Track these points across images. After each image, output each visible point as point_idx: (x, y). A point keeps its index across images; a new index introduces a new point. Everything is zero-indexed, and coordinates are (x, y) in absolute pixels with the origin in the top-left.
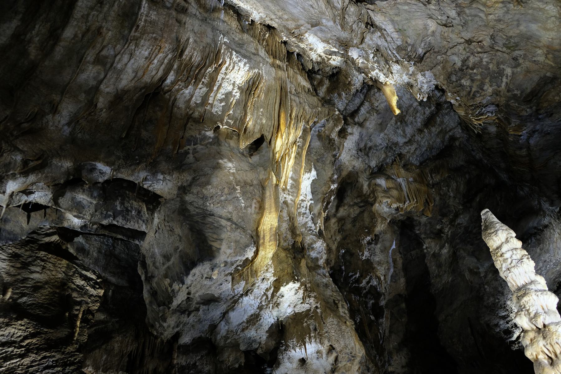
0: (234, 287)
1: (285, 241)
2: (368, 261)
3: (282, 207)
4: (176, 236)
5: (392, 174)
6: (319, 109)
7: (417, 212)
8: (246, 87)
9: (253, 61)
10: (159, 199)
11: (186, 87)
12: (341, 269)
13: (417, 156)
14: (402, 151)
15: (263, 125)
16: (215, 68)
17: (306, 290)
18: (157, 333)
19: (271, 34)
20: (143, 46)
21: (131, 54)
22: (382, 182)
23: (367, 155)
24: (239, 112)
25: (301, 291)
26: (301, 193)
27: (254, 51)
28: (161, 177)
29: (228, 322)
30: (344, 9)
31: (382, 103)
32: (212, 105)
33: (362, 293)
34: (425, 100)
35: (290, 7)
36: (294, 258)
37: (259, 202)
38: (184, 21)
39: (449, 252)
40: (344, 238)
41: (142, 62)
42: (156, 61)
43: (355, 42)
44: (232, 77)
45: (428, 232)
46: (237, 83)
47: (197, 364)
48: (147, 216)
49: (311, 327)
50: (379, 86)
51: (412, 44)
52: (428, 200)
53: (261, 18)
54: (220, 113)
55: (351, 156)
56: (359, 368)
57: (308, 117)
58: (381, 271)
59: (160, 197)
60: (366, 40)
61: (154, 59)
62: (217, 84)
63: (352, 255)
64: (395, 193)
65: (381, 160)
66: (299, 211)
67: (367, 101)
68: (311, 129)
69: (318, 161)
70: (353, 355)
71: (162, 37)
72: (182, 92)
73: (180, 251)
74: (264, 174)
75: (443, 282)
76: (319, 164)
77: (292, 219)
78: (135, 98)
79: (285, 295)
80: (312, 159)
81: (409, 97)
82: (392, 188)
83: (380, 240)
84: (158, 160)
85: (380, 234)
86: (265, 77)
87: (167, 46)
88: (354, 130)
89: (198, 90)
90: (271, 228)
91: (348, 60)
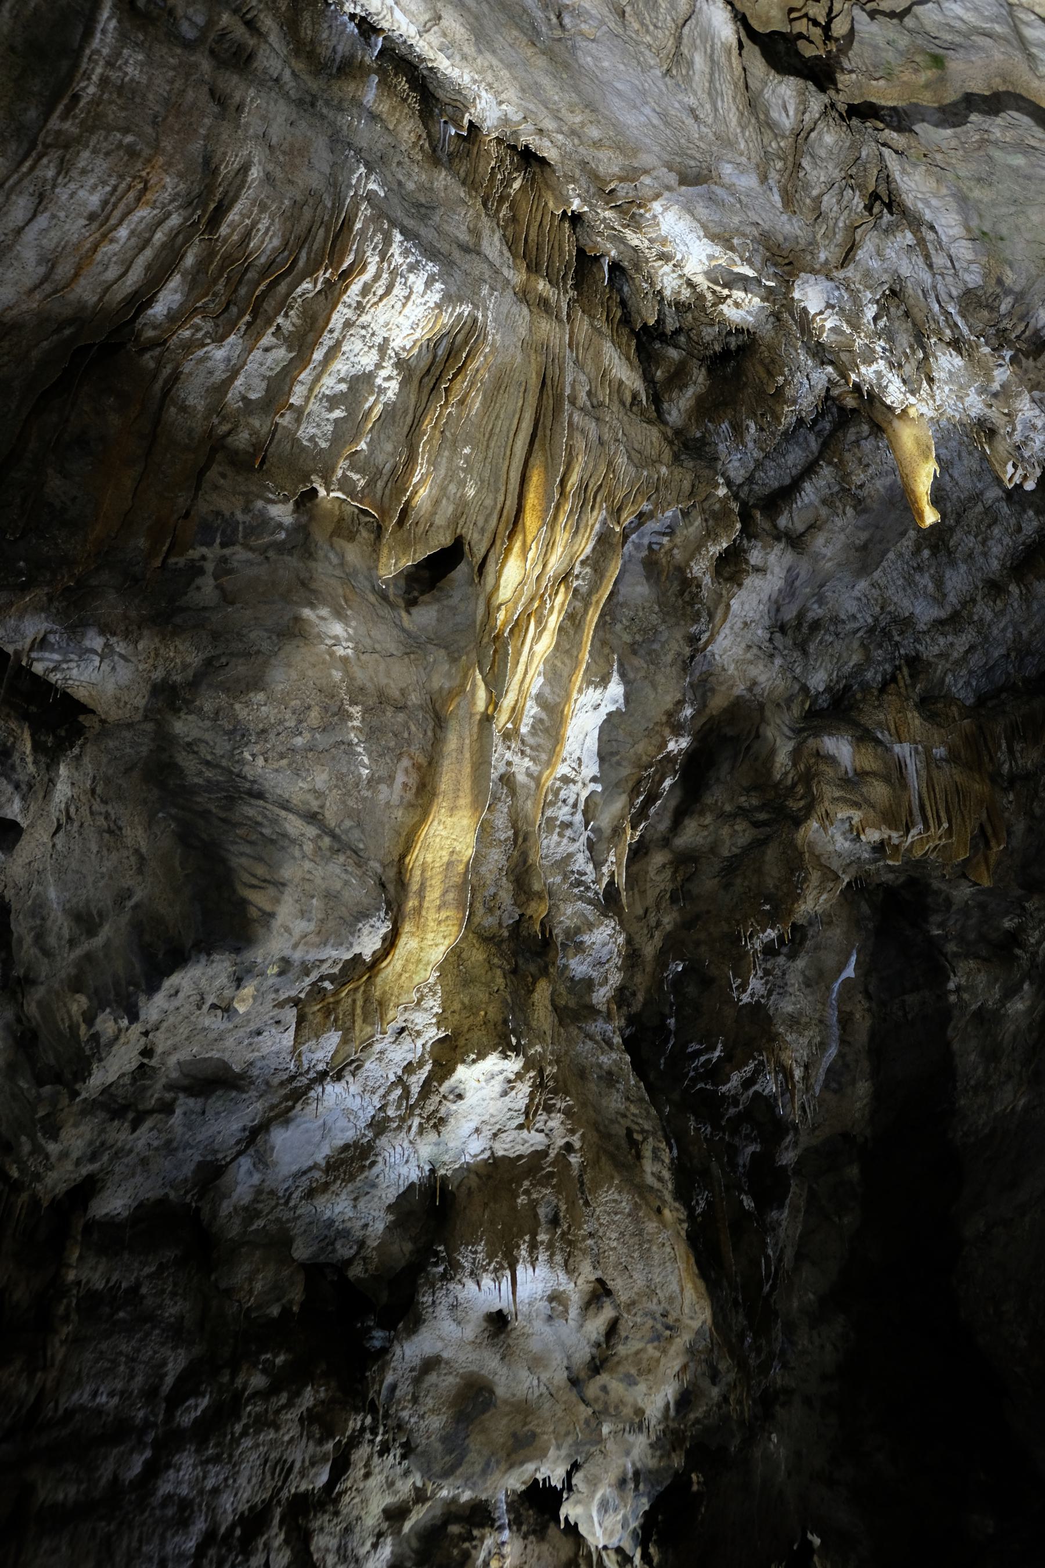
0: (304, 1048)
1: (490, 910)
2: (757, 1009)
3: (495, 790)
4: (126, 853)
5: (879, 724)
6: (664, 470)
7: (944, 866)
8: (424, 364)
9: (458, 275)
10: (81, 718)
11: (219, 339)
12: (663, 1026)
13: (971, 672)
14: (921, 648)
15: (466, 504)
16: (327, 281)
17: (539, 1086)
18: (21, 1171)
19: (531, 182)
20: (84, 172)
21: (41, 197)
22: (840, 748)
23: (802, 647)
24: (389, 447)
25: (524, 1088)
26: (565, 754)
27: (464, 237)
28: (95, 641)
29: (262, 1162)
30: (801, 136)
31: (880, 474)
32: (299, 412)
33: (722, 1116)
34: (1030, 486)
35: (616, 103)
36: (514, 971)
37: (418, 767)
38: (237, 98)
39: (1031, 1010)
40: (687, 924)
41: (75, 228)
42: (123, 232)
43: (822, 256)
44: (381, 321)
45: (972, 936)
46: (396, 344)
47: (144, 1290)
48: (31, 768)
49: (542, 1212)
50: (879, 418)
51: (1017, 288)
52: (989, 831)
53: (505, 120)
54: (324, 445)
55: (749, 647)
56: (685, 1368)
57: (620, 495)
58: (796, 1048)
59: (84, 709)
60: (860, 254)
61: (120, 223)
62: (327, 341)
63: (706, 982)
64: (879, 791)
65: (847, 669)
66: (549, 813)
67: (830, 463)
68: (625, 537)
69: (634, 649)
70: (670, 1320)
71: (156, 148)
72: (201, 353)
73: (136, 907)
74: (448, 675)
75: (998, 1109)
76: (637, 662)
77: (521, 839)
78: (35, 353)
79: (468, 1095)
80: (615, 642)
81: (975, 466)
82: (874, 774)
83: (808, 944)
84: (94, 582)
85: (811, 924)
86: (494, 335)
87: (168, 185)
88: (772, 558)
89: (257, 354)
90: (449, 864)
91: (781, 307)
